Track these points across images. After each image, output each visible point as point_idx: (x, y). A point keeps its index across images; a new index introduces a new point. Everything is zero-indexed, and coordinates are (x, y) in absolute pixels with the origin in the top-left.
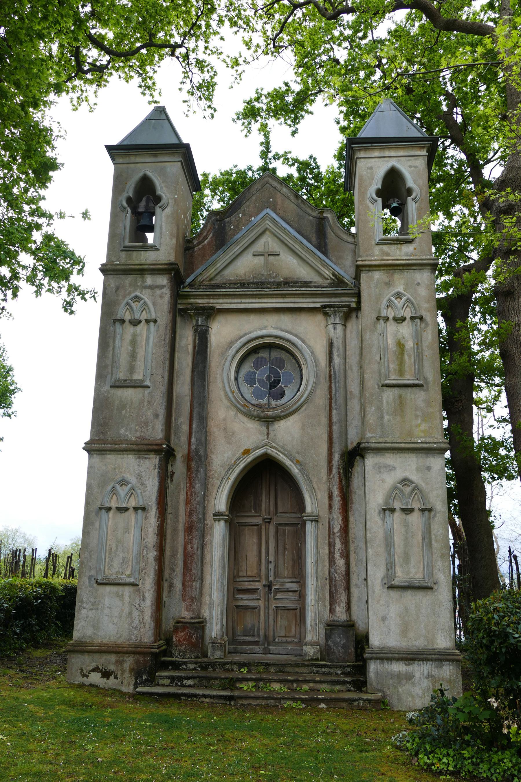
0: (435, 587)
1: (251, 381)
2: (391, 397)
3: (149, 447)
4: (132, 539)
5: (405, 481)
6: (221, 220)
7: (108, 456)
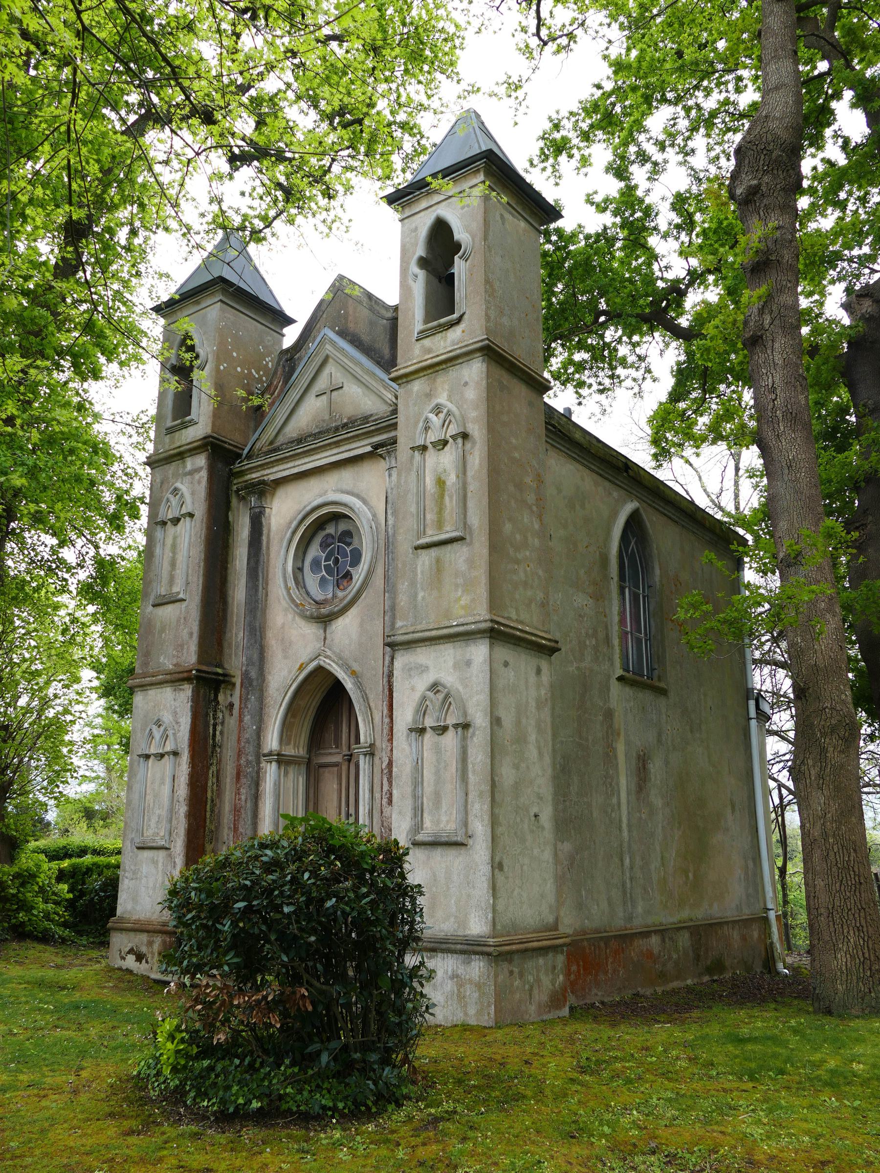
0: (471, 842)
2: (427, 563)
3: (181, 676)
5: (435, 687)
6: (291, 358)
7: (150, 692)
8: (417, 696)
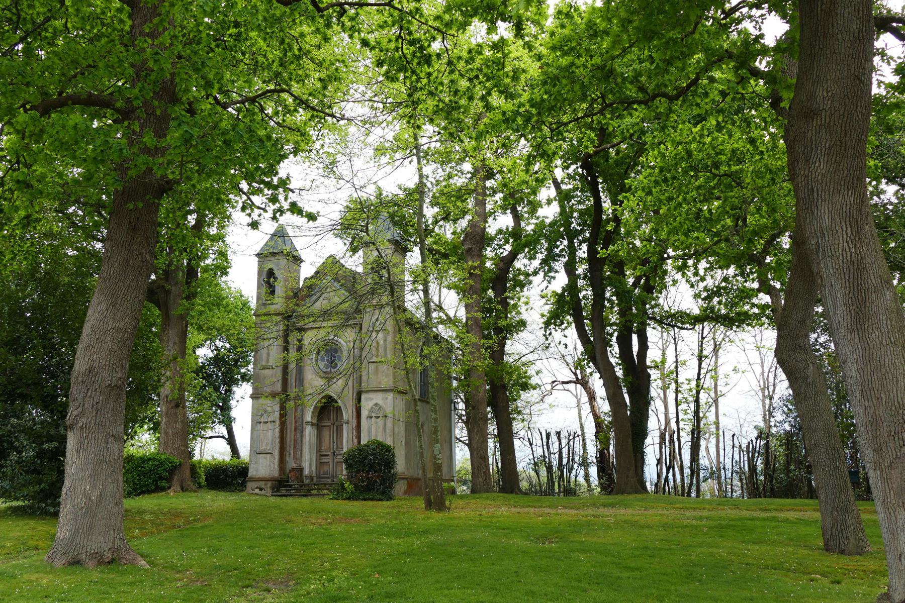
1: (323, 360)
4: (270, 433)
5: (376, 404)
8: (369, 407)
